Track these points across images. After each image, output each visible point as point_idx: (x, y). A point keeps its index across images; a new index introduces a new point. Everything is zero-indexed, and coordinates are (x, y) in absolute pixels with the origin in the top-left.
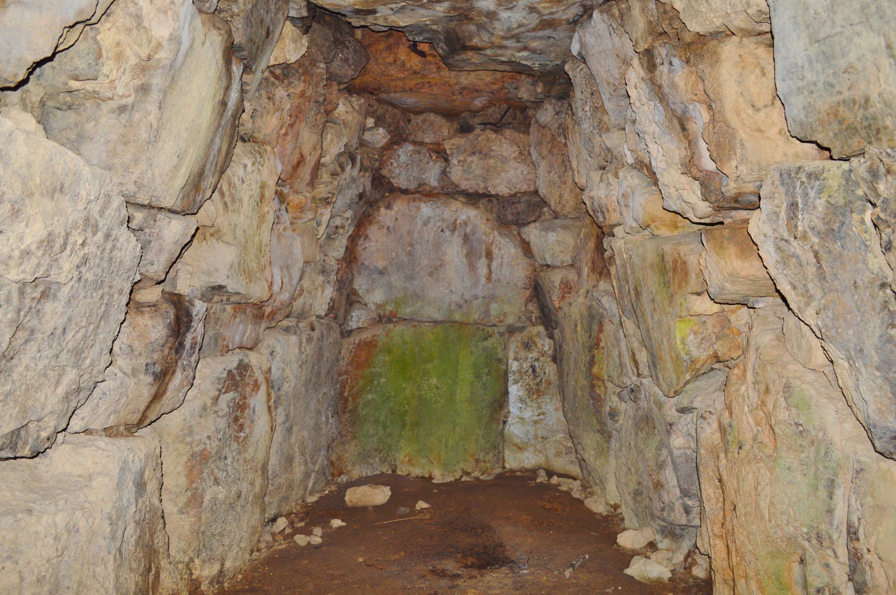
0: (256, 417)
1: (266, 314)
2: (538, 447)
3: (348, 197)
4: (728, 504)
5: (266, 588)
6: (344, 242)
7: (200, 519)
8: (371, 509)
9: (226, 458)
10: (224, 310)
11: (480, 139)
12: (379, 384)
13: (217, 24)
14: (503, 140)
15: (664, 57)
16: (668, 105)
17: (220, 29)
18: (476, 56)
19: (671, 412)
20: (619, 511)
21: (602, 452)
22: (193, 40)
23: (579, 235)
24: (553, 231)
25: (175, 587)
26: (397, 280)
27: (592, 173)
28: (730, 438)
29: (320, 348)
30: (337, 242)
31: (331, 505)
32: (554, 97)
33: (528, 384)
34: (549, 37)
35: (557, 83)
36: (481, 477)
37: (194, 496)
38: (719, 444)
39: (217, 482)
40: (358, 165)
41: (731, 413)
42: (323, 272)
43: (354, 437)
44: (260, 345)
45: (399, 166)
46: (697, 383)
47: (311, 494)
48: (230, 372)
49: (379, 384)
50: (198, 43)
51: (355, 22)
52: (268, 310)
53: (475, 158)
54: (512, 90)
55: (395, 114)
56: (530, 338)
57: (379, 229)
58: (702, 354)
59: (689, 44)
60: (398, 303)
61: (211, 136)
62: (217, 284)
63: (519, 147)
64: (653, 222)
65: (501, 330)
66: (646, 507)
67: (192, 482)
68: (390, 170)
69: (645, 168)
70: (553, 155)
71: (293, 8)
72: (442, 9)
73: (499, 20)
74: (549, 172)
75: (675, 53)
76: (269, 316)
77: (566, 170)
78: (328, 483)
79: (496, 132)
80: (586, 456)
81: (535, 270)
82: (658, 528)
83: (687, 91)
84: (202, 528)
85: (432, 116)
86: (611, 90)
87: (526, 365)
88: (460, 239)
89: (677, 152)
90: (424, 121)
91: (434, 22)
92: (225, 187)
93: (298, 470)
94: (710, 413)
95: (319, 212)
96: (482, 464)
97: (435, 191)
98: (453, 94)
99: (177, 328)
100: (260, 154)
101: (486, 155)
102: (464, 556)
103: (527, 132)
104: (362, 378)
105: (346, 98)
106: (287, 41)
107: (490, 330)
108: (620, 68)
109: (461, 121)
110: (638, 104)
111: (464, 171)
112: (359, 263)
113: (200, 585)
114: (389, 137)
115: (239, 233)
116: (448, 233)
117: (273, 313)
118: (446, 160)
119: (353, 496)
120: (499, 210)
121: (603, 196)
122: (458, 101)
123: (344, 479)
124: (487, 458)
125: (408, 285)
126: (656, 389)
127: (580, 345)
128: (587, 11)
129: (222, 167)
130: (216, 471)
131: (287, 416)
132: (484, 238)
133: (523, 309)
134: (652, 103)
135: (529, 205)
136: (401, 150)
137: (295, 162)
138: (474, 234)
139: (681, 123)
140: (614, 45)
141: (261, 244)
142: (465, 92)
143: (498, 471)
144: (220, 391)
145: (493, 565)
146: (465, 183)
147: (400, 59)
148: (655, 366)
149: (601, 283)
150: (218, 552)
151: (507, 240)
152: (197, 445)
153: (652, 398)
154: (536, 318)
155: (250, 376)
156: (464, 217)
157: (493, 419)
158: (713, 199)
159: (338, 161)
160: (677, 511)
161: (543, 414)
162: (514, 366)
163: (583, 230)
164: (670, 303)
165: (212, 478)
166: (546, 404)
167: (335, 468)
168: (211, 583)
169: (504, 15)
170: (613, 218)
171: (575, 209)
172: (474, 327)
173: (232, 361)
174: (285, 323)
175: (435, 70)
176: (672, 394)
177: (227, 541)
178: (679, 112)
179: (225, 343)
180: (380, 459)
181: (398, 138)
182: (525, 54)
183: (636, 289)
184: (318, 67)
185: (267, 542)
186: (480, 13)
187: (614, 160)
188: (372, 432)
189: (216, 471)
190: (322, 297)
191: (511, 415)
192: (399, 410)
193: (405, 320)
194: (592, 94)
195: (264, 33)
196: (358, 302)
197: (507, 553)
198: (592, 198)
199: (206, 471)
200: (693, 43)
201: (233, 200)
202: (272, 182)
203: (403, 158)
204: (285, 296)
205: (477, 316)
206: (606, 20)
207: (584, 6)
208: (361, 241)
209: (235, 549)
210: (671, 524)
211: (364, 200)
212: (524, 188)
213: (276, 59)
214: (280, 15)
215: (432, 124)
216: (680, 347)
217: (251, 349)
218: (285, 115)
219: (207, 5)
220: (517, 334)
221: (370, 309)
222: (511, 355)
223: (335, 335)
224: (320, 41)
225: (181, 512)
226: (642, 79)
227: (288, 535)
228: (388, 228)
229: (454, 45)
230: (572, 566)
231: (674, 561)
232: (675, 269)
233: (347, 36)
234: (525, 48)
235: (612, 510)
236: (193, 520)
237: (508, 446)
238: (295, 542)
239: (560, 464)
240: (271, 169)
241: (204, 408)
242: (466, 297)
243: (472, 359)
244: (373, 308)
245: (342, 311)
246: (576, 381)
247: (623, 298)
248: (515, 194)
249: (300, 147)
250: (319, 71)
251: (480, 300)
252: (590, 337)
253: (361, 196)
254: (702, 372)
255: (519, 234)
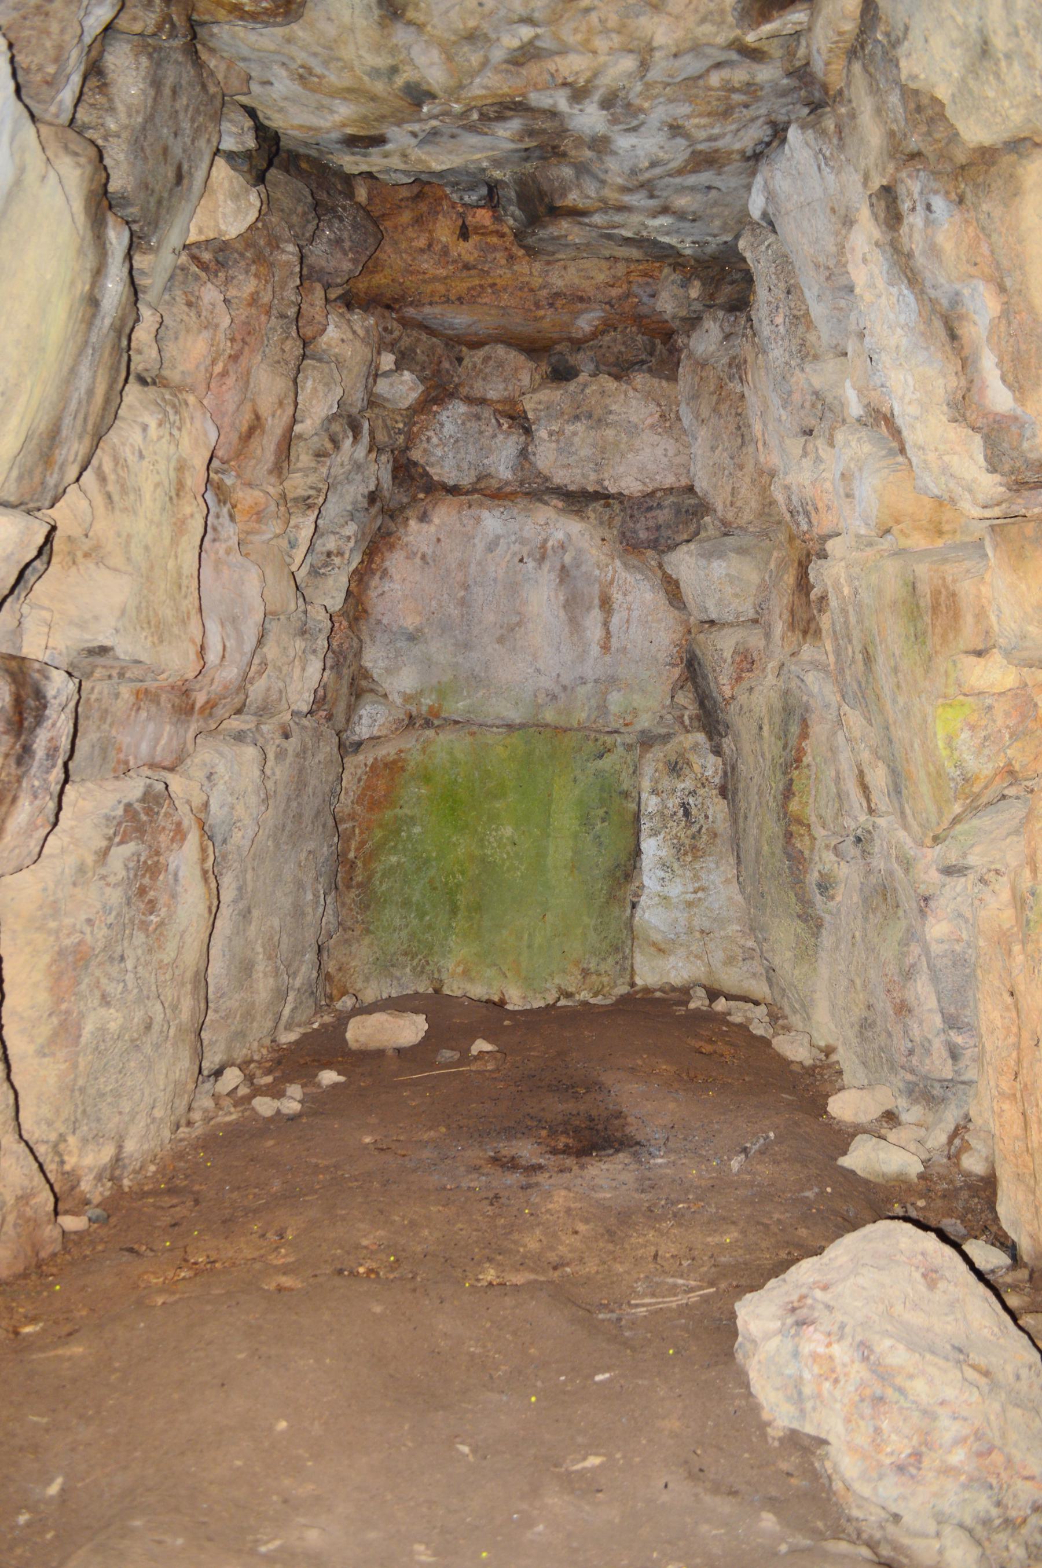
0: (179, 889)
1: (198, 706)
2: (693, 948)
3: (349, 498)
4: (1026, 1035)
5: (196, 1188)
6: (344, 580)
7: (75, 1066)
8: (390, 1053)
9: (122, 958)
10: (117, 695)
11: (587, 391)
12: (409, 837)
13: (72, 146)
14: (631, 393)
15: (916, 196)
16: (922, 292)
17: (76, 154)
18: (576, 229)
19: (929, 876)
20: (834, 1058)
21: (806, 953)
22: (22, 170)
23: (767, 563)
24: (719, 558)
25: (26, 1183)
26: (439, 650)
27: (787, 441)
28: (1032, 916)
29: (301, 771)
30: (330, 581)
31: (325, 1047)
32: (721, 307)
33: (676, 836)
34: (709, 188)
35: (726, 280)
36: (592, 1001)
37: (63, 1024)
38: (1012, 927)
39: (105, 1000)
40: (365, 438)
41: (1034, 871)
42: (303, 632)
43: (368, 931)
44: (188, 761)
45: (442, 443)
46: (975, 822)
47: (288, 1028)
48: (128, 806)
49: (409, 837)
50: (31, 177)
51: (350, 162)
52: (200, 699)
53: (579, 427)
54: (645, 299)
55: (433, 348)
56: (681, 755)
57: (407, 558)
58: (983, 767)
59: (963, 167)
60: (441, 692)
61: (69, 361)
62: (96, 644)
63: (659, 405)
64: (898, 522)
65: (628, 741)
66: (881, 1049)
67: (60, 1000)
68: (425, 450)
69: (881, 420)
70: (720, 416)
71: (230, 134)
72: (508, 134)
73: (614, 153)
74: (713, 449)
75: (935, 185)
76: (203, 709)
77: (743, 443)
78: (318, 1010)
79: (617, 378)
80: (776, 962)
81: (689, 632)
82: (901, 1085)
83: (958, 257)
84: (81, 1082)
85: (501, 350)
86: (822, 278)
87: (673, 803)
88: (553, 576)
89: (941, 381)
90: (487, 359)
91: (497, 163)
92: (108, 467)
93: (263, 987)
94: (997, 872)
95: (292, 523)
96: (594, 977)
97: (508, 489)
98: (537, 305)
99: (16, 718)
100: (174, 406)
101: (600, 420)
102: (553, 1133)
103: (673, 378)
104: (381, 826)
105: (342, 315)
106: (221, 197)
107: (609, 739)
108: (837, 234)
109: (553, 360)
110: (868, 297)
111: (560, 451)
112: (372, 621)
113: (79, 1182)
114: (421, 388)
115: (137, 552)
116: (531, 564)
117: (210, 706)
118: (528, 431)
119: (360, 1033)
120: (624, 522)
121: (807, 483)
122: (549, 321)
123: (347, 1003)
124: (603, 967)
125: (460, 659)
126: (902, 834)
127: (768, 763)
128: (778, 133)
129: (97, 427)
130: (104, 981)
131: (240, 889)
132: (597, 572)
133: (668, 702)
134: (894, 290)
135: (678, 512)
136: (445, 413)
137: (244, 428)
138: (578, 566)
139: (948, 325)
140: (825, 189)
141: (180, 575)
142: (559, 303)
143: (623, 989)
144: (110, 839)
145: (604, 1149)
146: (562, 473)
147: (439, 241)
148: (898, 792)
149: (805, 647)
150: (111, 1125)
151: (639, 577)
152: (69, 935)
153: (893, 852)
154: (691, 718)
155: (167, 815)
156: (560, 535)
157: (612, 898)
158: (1007, 468)
159: (327, 430)
160: (935, 1056)
161: (703, 889)
162: (651, 804)
163: (775, 554)
164: (927, 672)
165: (97, 994)
166: (709, 872)
167: (327, 986)
168: (99, 1178)
169: (623, 142)
170: (825, 523)
171: (761, 515)
172: (580, 735)
173: (133, 789)
174: (235, 724)
175: (503, 262)
176: (928, 841)
177: (126, 1106)
178: (945, 302)
179: (122, 756)
180: (413, 969)
181: (438, 392)
182: (664, 221)
183: (866, 651)
184: (283, 251)
185: (205, 1110)
186: (579, 142)
187: (828, 414)
188: (397, 922)
189: (104, 981)
190: (303, 678)
191: (646, 891)
192: (446, 884)
193: (456, 722)
194: (788, 293)
195: (171, 174)
196: (372, 691)
197: (628, 1130)
198: (787, 488)
199: (86, 981)
200: (970, 164)
201: (124, 490)
202: (199, 462)
203: (449, 428)
204: (231, 673)
205: (584, 715)
206: (812, 142)
207: (773, 124)
208: (375, 581)
209: (142, 1122)
210: (926, 1078)
211: (378, 504)
212: (669, 481)
213: (200, 231)
214: (202, 143)
215: (501, 364)
216: (945, 753)
217: (171, 769)
218: (221, 336)
219: (53, 109)
220: (656, 749)
221: (393, 702)
222: (646, 784)
223: (328, 748)
224: (286, 203)
225: (41, 1053)
226: (877, 244)
227: (242, 1098)
228: (423, 557)
229: (533, 204)
230: (745, 1150)
231: (929, 1144)
232: (935, 608)
233: (340, 198)
234: (665, 210)
235: (822, 1056)
236: (63, 1066)
237: (640, 946)
238: (253, 1109)
239: (731, 978)
240: (196, 438)
241: (81, 869)
242: (565, 680)
243: (577, 792)
244: (399, 701)
245: (342, 706)
246: (760, 827)
247: (841, 671)
248: (653, 492)
249: (253, 401)
250: (284, 257)
251: (590, 686)
252: (785, 748)
253: (372, 497)
254: (984, 800)
255: (660, 566)
